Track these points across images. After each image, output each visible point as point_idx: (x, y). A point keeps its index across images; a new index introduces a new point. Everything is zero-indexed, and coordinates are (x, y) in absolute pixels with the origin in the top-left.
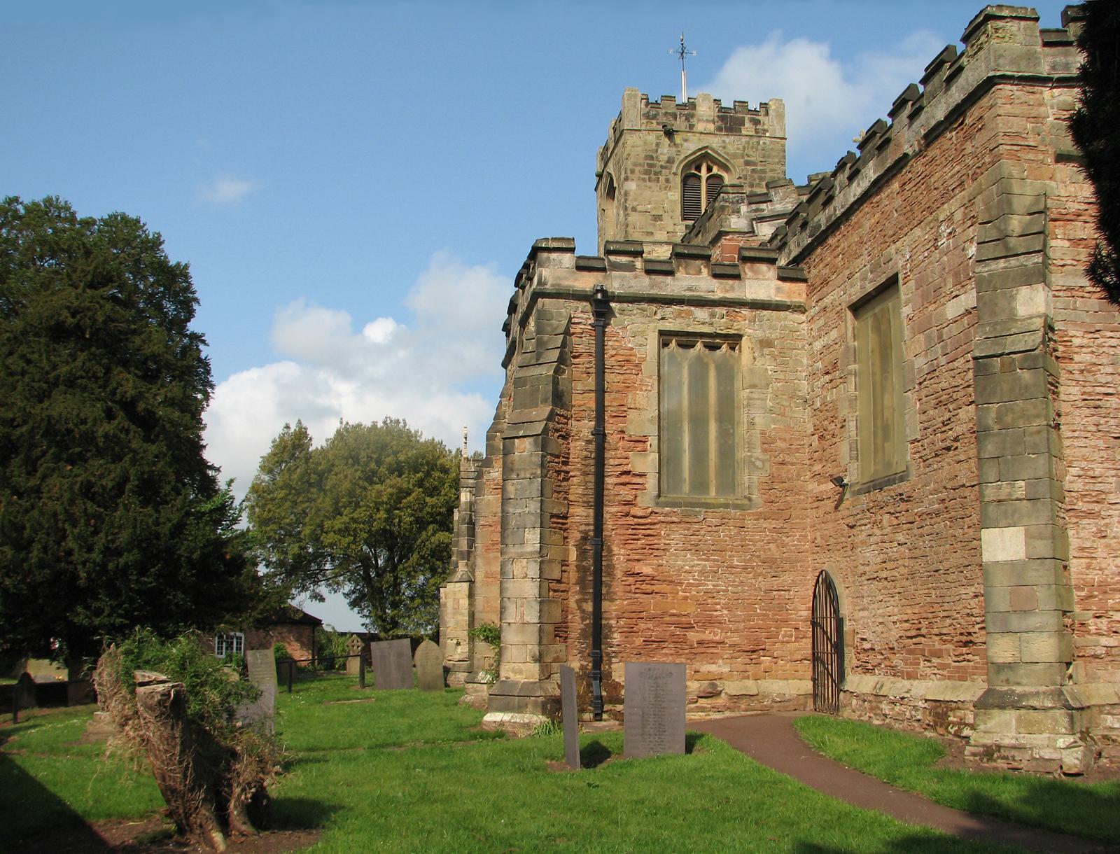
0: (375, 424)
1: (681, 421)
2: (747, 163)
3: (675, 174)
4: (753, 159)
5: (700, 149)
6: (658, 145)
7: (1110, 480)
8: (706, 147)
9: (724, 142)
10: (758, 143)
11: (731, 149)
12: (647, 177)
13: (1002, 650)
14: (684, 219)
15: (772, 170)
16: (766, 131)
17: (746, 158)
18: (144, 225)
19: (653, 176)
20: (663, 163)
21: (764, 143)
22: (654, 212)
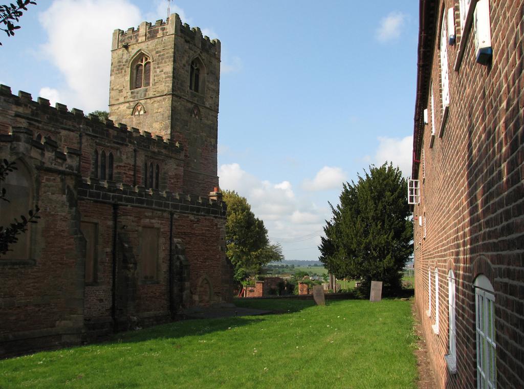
0: (343, 193)
1: (517, 205)
2: (157, 52)
3: (128, 67)
4: (159, 49)
5: (138, 51)
6: (123, 55)
7: (53, 304)
8: (140, 50)
9: (148, 44)
10: (162, 40)
11: (151, 47)
12: (117, 72)
13: (247, 350)
14: (130, 90)
15: (167, 53)
16: (167, 32)
17: (156, 50)
18: (234, 192)
19: (120, 71)
20: (124, 63)
21: (165, 40)
22: (120, 89)
